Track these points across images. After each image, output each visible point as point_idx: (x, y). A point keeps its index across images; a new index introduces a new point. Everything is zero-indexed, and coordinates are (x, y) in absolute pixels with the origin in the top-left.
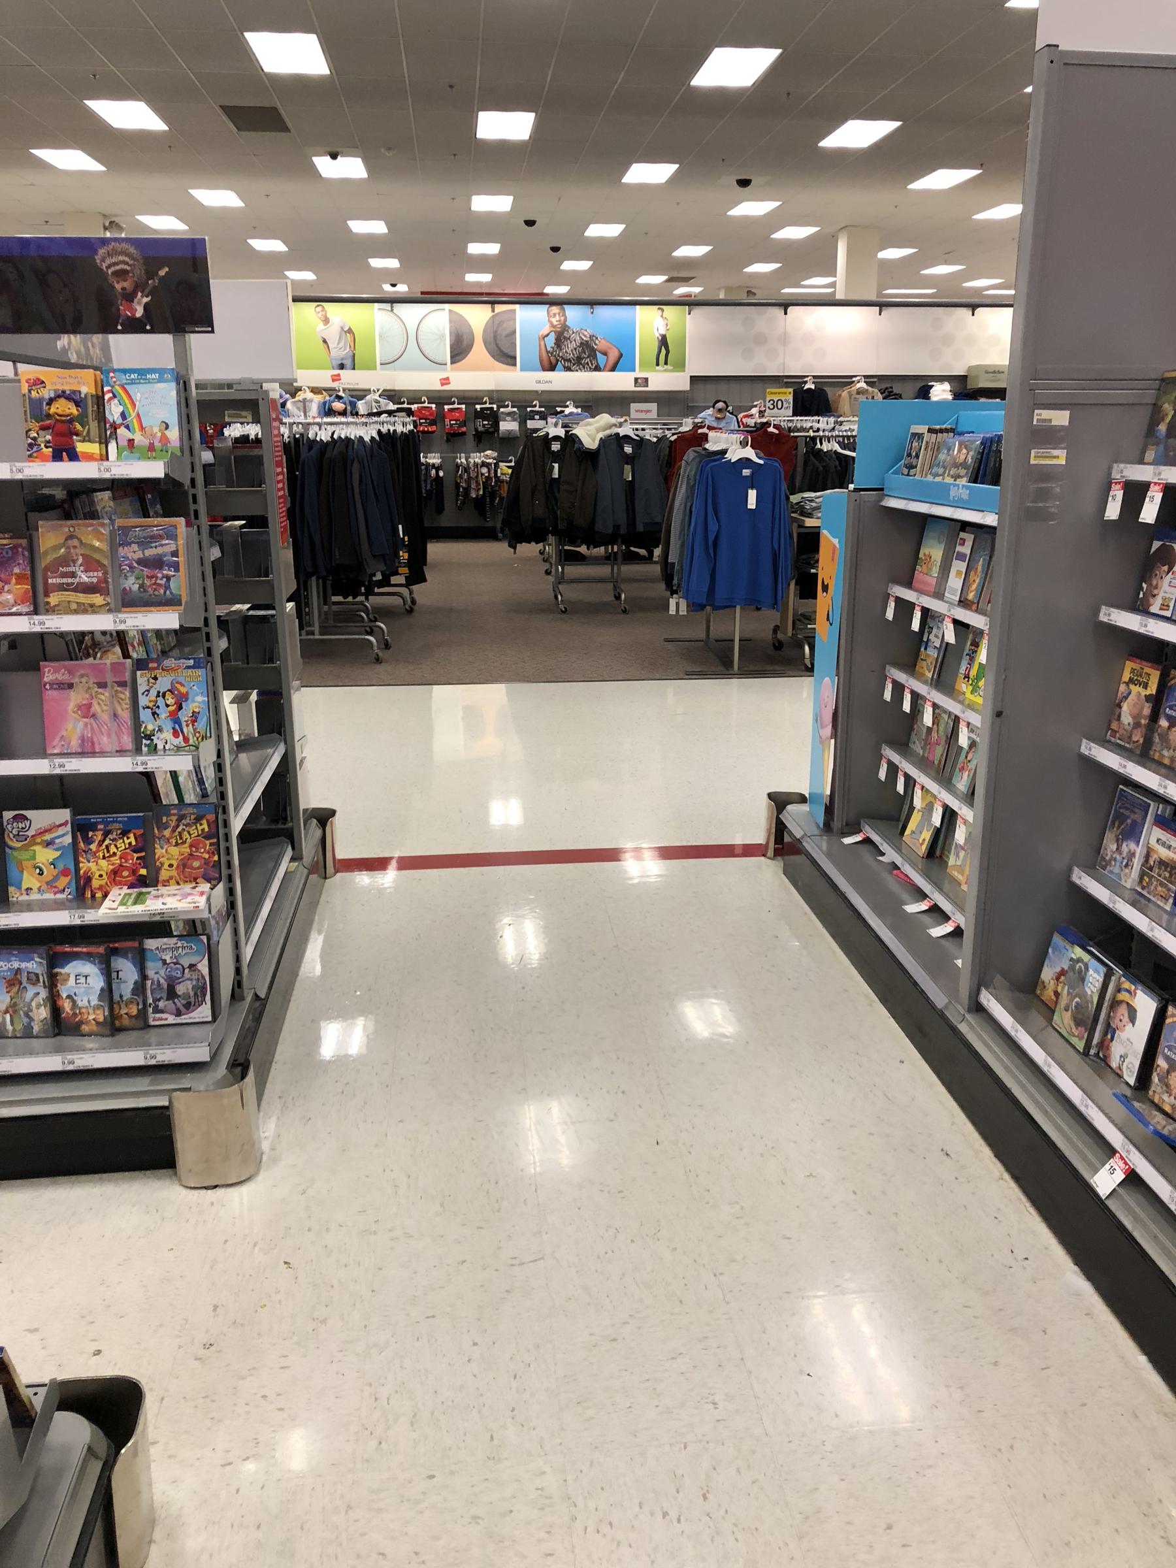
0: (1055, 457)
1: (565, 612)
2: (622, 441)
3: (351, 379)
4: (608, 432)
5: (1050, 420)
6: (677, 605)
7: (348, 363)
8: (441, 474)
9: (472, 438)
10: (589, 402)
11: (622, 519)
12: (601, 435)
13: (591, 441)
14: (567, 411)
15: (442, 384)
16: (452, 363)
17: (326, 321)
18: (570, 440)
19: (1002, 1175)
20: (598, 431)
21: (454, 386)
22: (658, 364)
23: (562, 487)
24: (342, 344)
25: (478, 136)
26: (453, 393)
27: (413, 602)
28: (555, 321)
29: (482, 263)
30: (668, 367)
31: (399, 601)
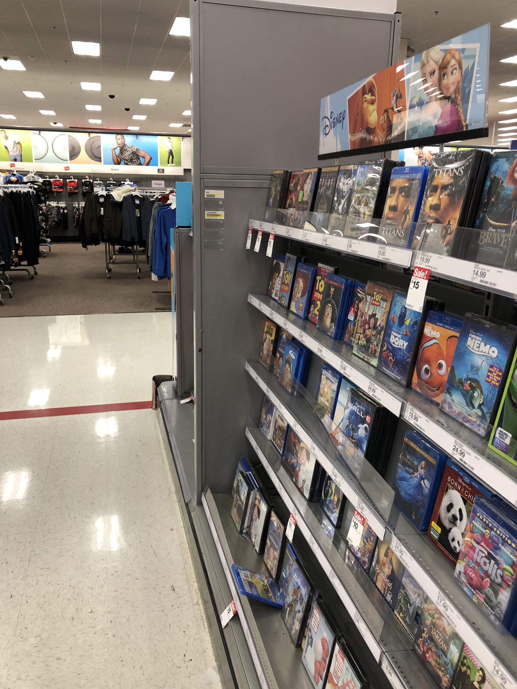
0: (218, 215)
1: (110, 278)
2: (134, 198)
3: (19, 166)
4: (128, 194)
5: (214, 196)
6: (154, 277)
7: (18, 158)
8: (66, 211)
9: (81, 194)
10: (137, 179)
11: (135, 234)
12: (124, 195)
13: (119, 198)
14: (126, 183)
15: (66, 170)
16: (70, 160)
17: (6, 138)
18: (109, 197)
19: (198, 601)
20: (123, 193)
21: (71, 171)
22: (168, 163)
23: (105, 219)
24: (15, 149)
26: (72, 174)
27: (36, 273)
28: (119, 142)
29: (94, 115)
30: (173, 164)
31: (26, 273)
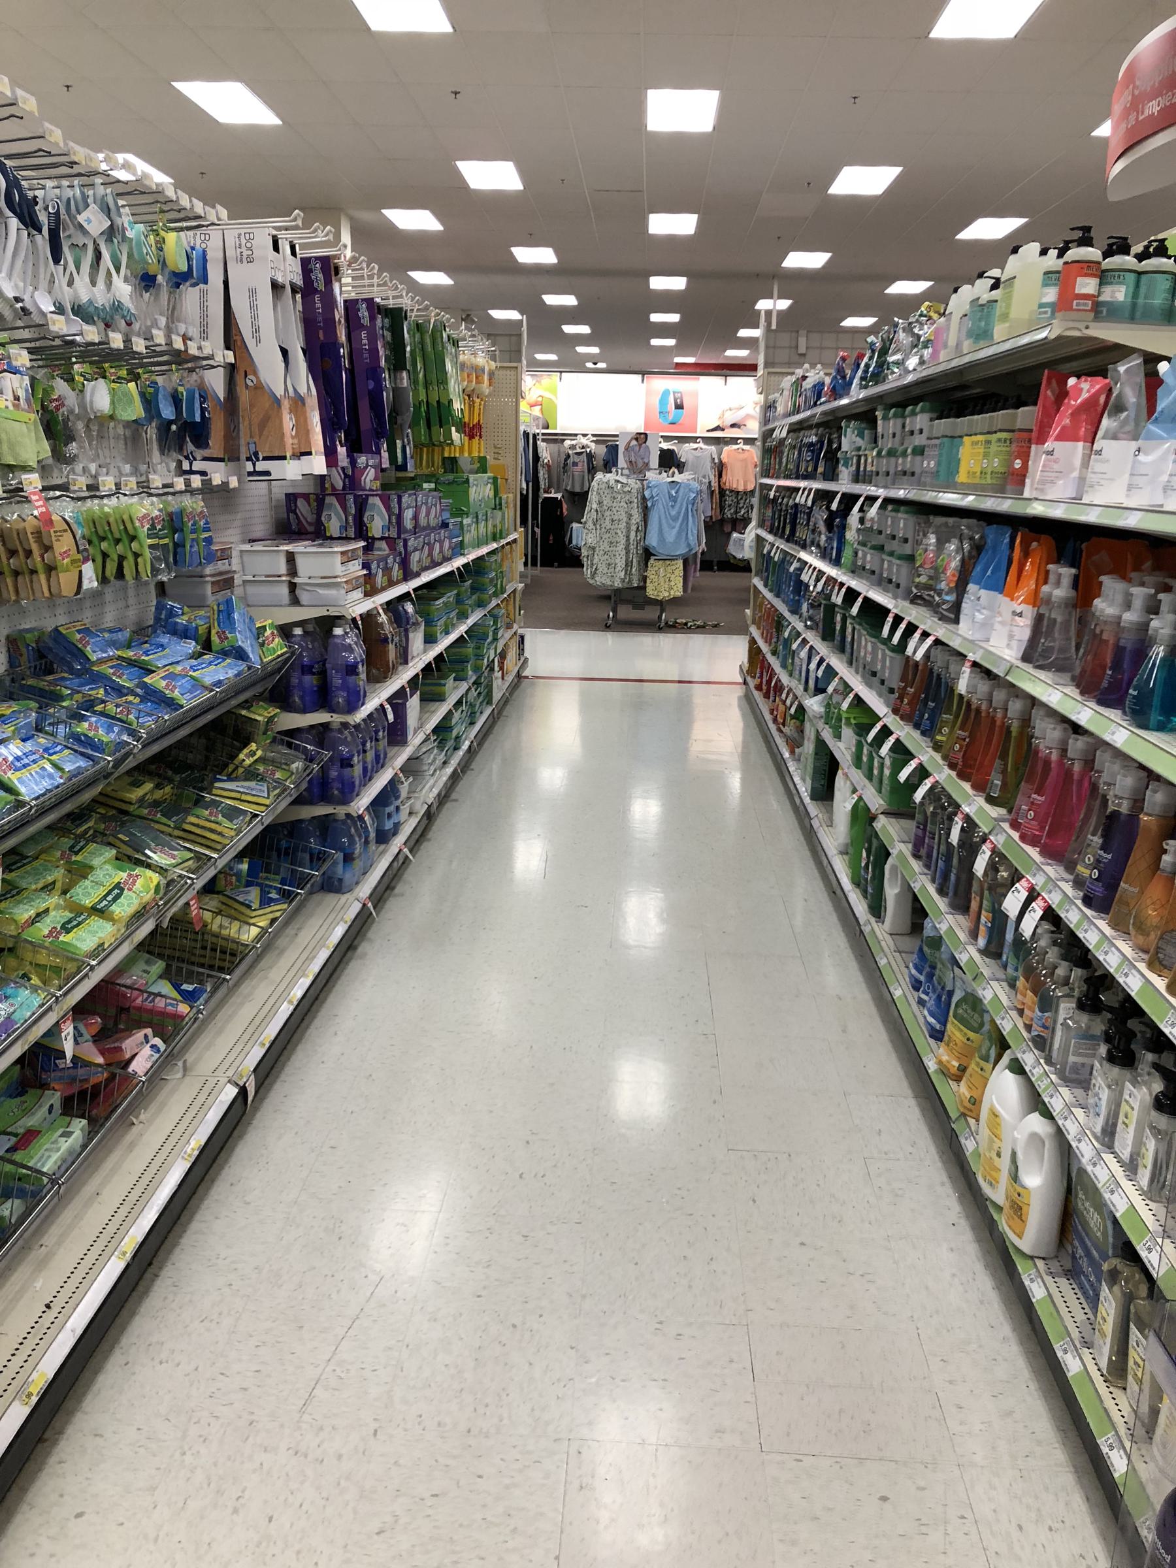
25: (649, 91)
